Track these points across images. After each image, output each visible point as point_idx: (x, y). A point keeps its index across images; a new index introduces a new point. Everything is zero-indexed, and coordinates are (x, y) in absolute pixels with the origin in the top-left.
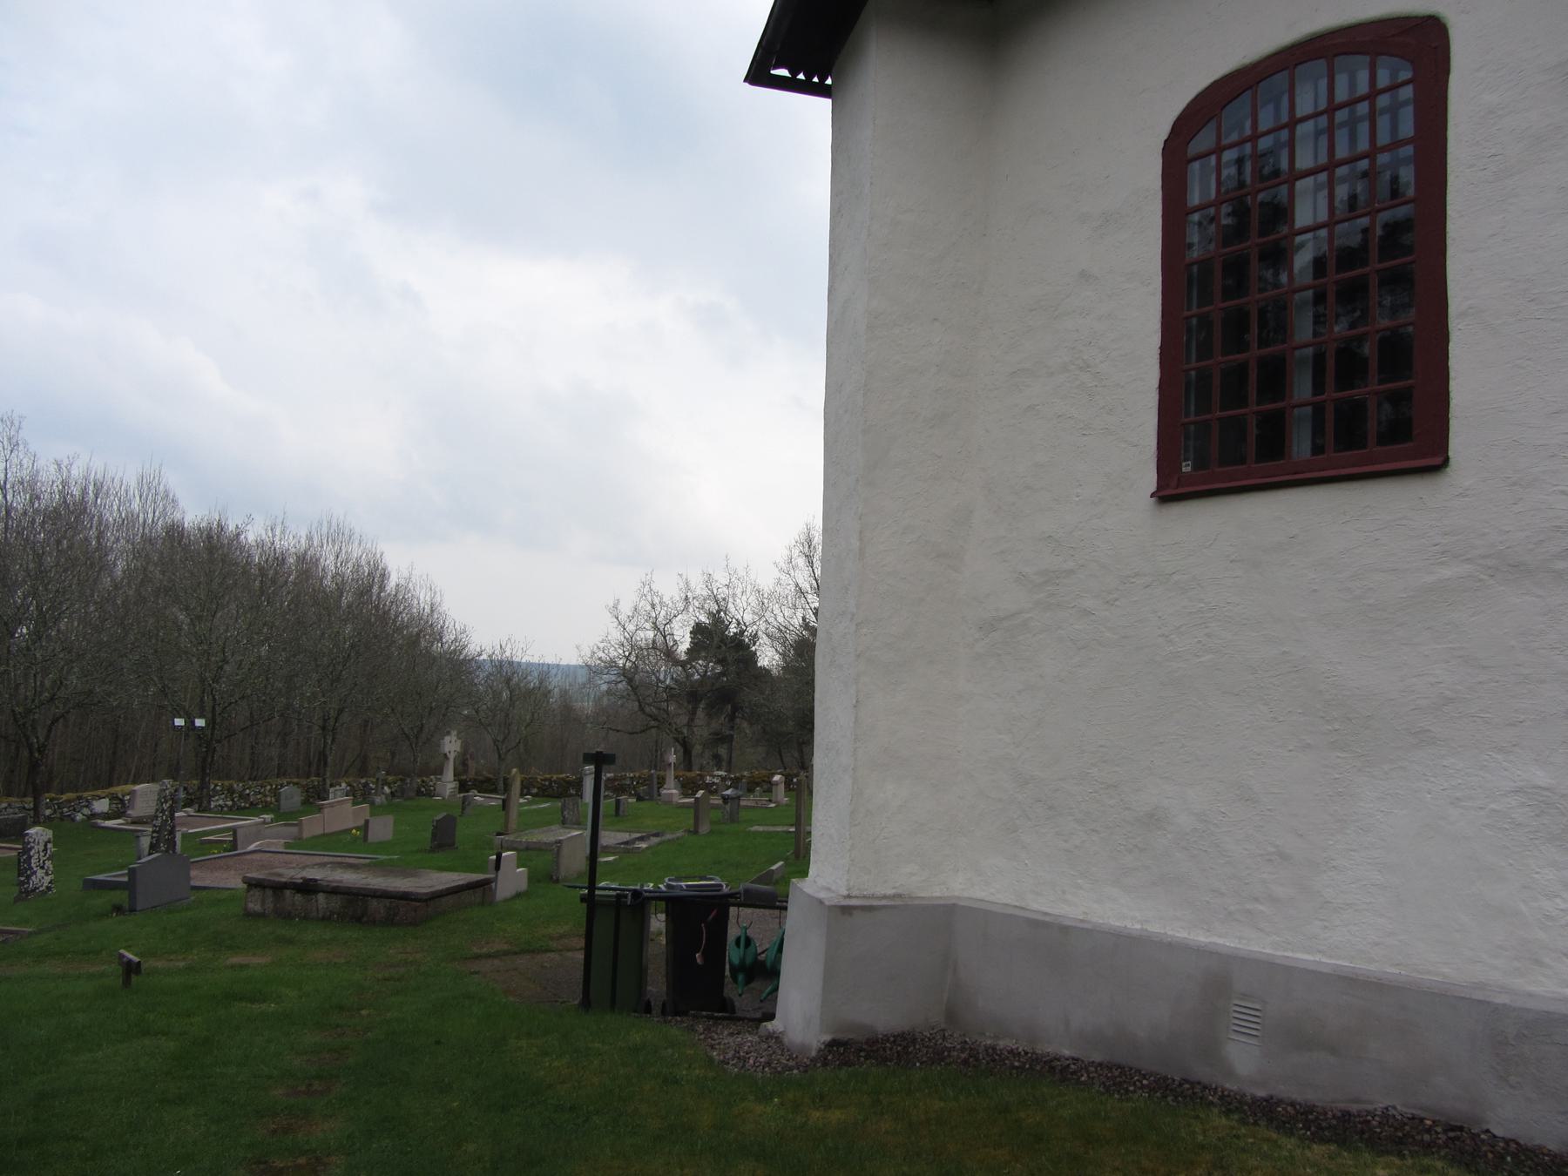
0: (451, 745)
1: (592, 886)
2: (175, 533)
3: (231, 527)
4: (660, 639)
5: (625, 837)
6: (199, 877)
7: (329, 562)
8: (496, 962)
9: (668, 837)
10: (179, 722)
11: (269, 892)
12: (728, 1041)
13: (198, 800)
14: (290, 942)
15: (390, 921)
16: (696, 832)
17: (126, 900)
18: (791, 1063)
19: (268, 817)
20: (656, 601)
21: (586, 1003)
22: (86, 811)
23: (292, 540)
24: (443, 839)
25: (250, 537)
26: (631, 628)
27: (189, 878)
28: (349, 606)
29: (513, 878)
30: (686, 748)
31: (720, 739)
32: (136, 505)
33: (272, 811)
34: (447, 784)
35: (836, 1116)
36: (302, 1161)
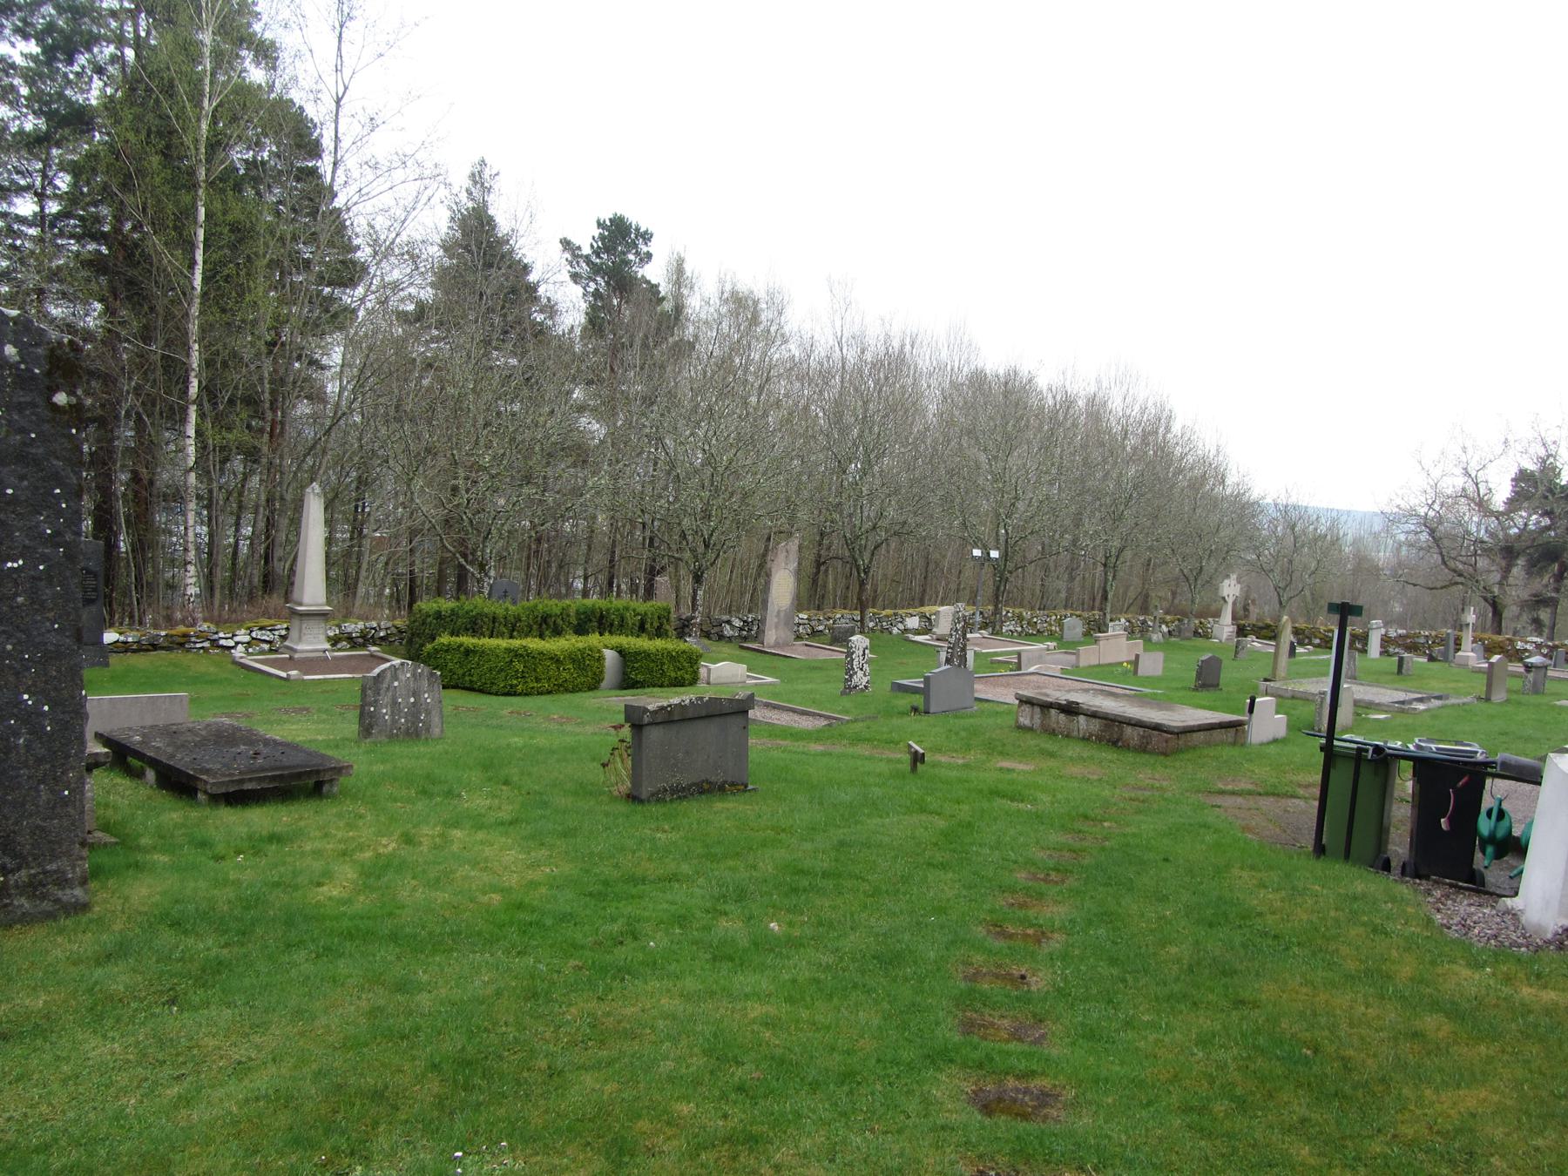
0: (1230, 589)
1: (1331, 734)
2: (978, 380)
3: (1024, 372)
4: (1471, 489)
5: (1401, 696)
6: (982, 691)
7: (1116, 404)
8: (1240, 800)
9: (1452, 701)
10: (977, 553)
11: (1037, 710)
12: (1464, 906)
13: (991, 624)
14: (1052, 755)
15: (1143, 748)
16: (1488, 699)
17: (921, 702)
18: (1520, 941)
19: (1052, 644)
20: (1468, 444)
21: (1320, 850)
22: (901, 626)
23: (1081, 387)
24: (1207, 679)
25: (1042, 383)
26: (1436, 473)
27: (972, 691)
28: (1135, 449)
29: (1268, 723)
30: (1496, 608)
31: (1539, 601)
32: (944, 355)
33: (1056, 639)
34: (1225, 628)
35: (1549, 996)
36: (1030, 931)
